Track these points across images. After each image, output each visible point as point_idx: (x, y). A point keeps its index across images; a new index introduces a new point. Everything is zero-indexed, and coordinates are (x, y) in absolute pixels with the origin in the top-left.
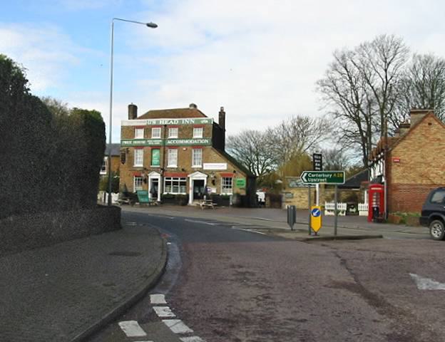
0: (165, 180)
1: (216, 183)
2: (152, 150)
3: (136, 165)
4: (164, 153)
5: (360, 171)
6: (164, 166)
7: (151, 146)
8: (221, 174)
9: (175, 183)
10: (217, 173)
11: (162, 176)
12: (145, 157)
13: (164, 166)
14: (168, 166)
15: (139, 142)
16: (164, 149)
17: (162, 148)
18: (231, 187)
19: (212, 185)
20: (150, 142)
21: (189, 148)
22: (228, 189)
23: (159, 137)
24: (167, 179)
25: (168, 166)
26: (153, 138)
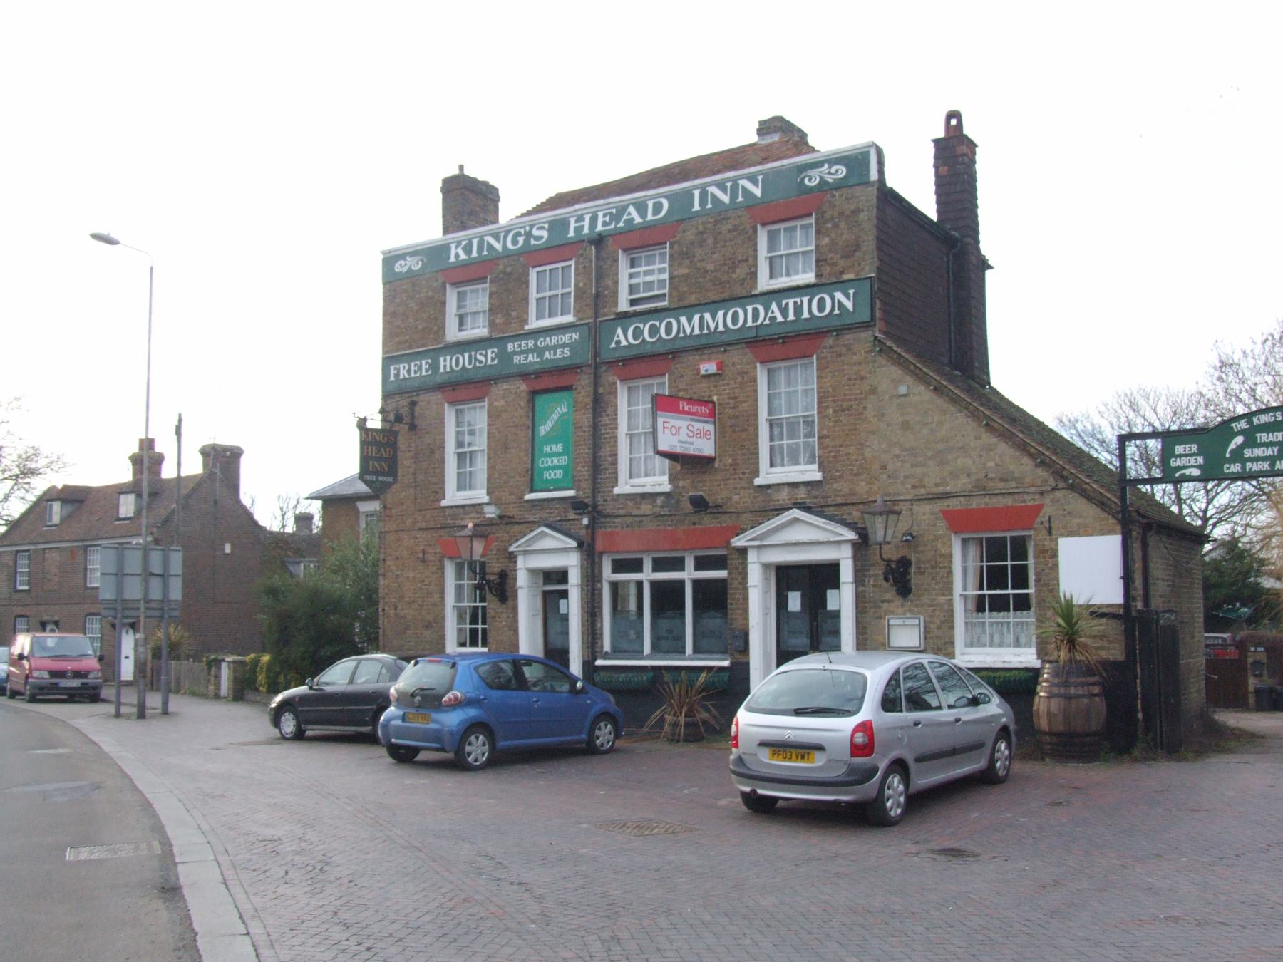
0: (608, 574)
1: (915, 579)
2: (534, 393)
3: (453, 496)
4: (596, 355)
5: (889, 625)
6: (595, 490)
7: (524, 375)
8: (948, 515)
9: (920, 327)
10: (925, 512)
11: (589, 551)
12: (498, 446)
13: (595, 490)
14: (617, 491)
15: (464, 360)
16: (597, 377)
17: (584, 381)
18: (1023, 604)
19: (890, 593)
20: (524, 356)
21: (737, 357)
22: (1011, 617)
23: (569, 318)
24: (619, 566)
25: (617, 491)
26: (534, 324)
